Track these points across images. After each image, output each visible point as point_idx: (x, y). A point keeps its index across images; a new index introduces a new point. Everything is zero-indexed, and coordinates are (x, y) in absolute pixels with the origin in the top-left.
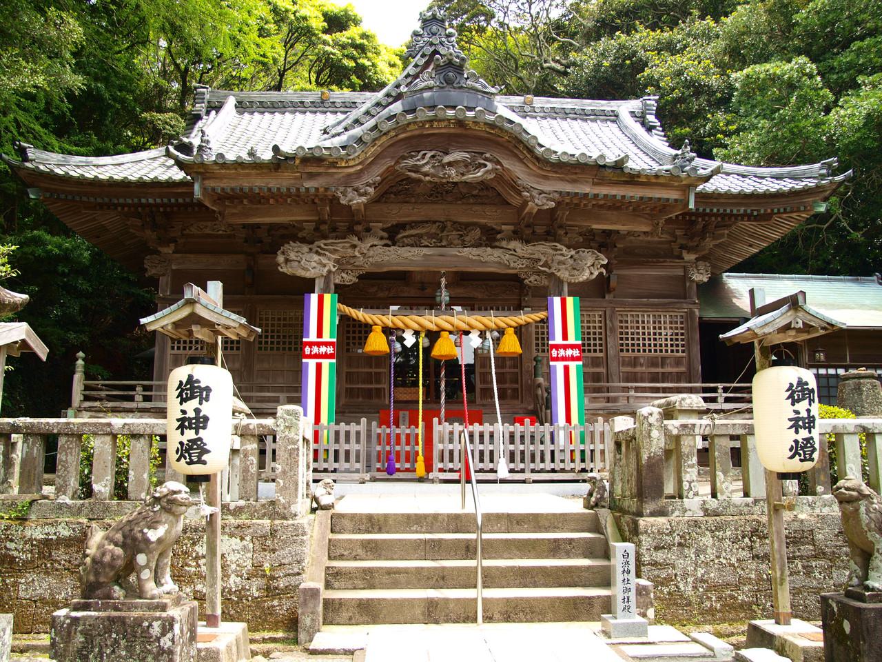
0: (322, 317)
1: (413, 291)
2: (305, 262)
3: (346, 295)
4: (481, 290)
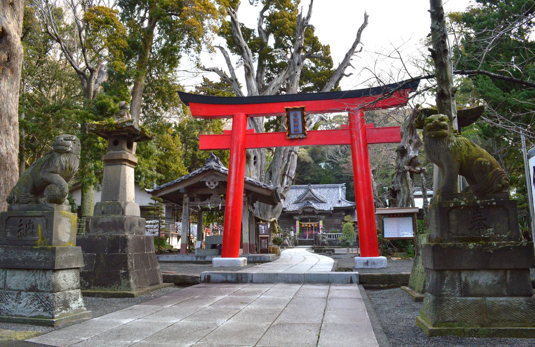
0: (298, 223)
1: (306, 220)
2: (296, 218)
3: (300, 221)
4: (313, 220)
